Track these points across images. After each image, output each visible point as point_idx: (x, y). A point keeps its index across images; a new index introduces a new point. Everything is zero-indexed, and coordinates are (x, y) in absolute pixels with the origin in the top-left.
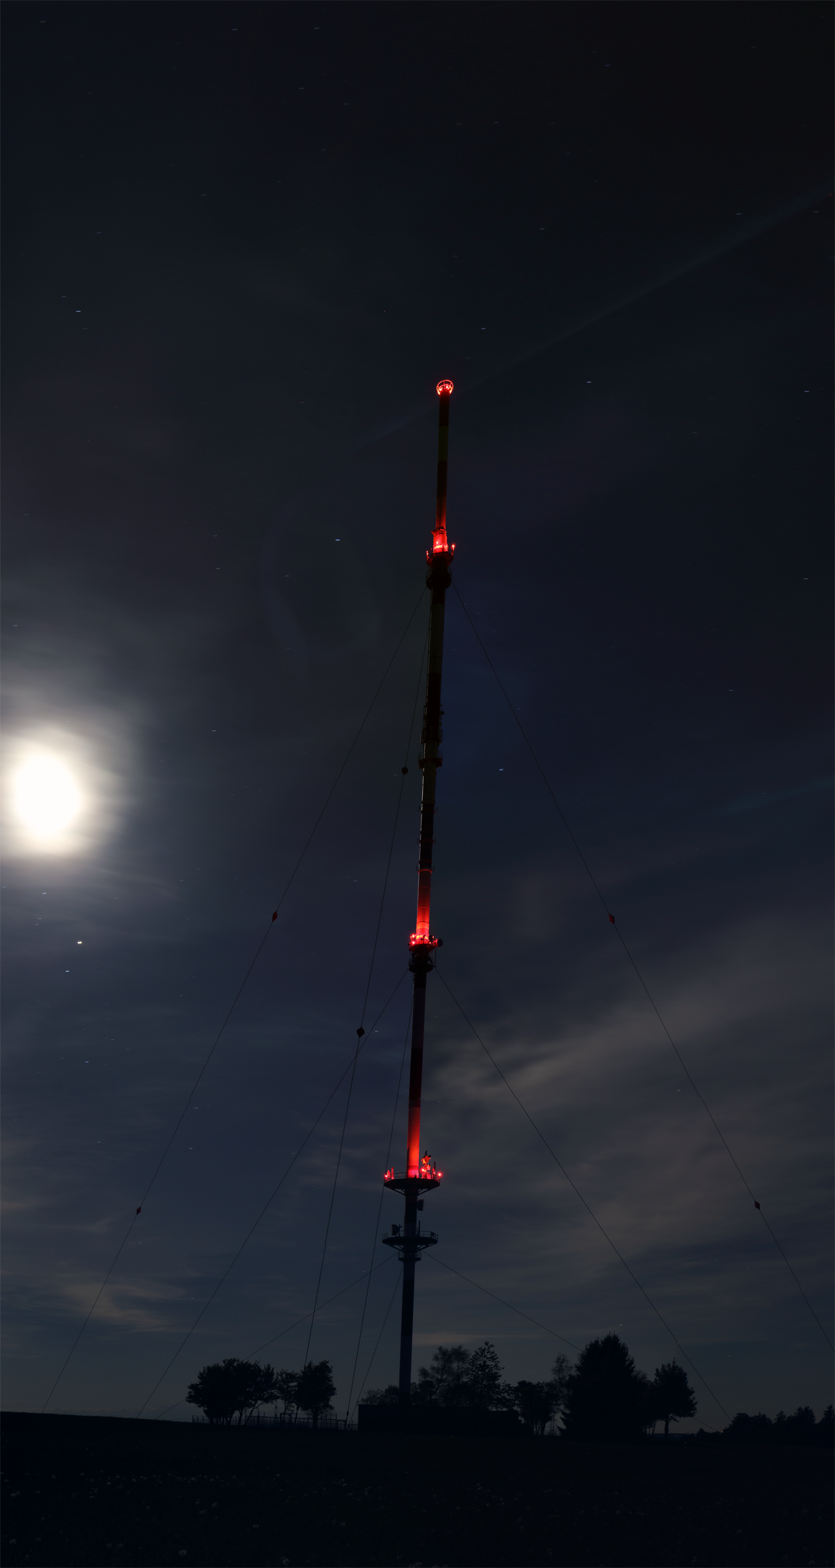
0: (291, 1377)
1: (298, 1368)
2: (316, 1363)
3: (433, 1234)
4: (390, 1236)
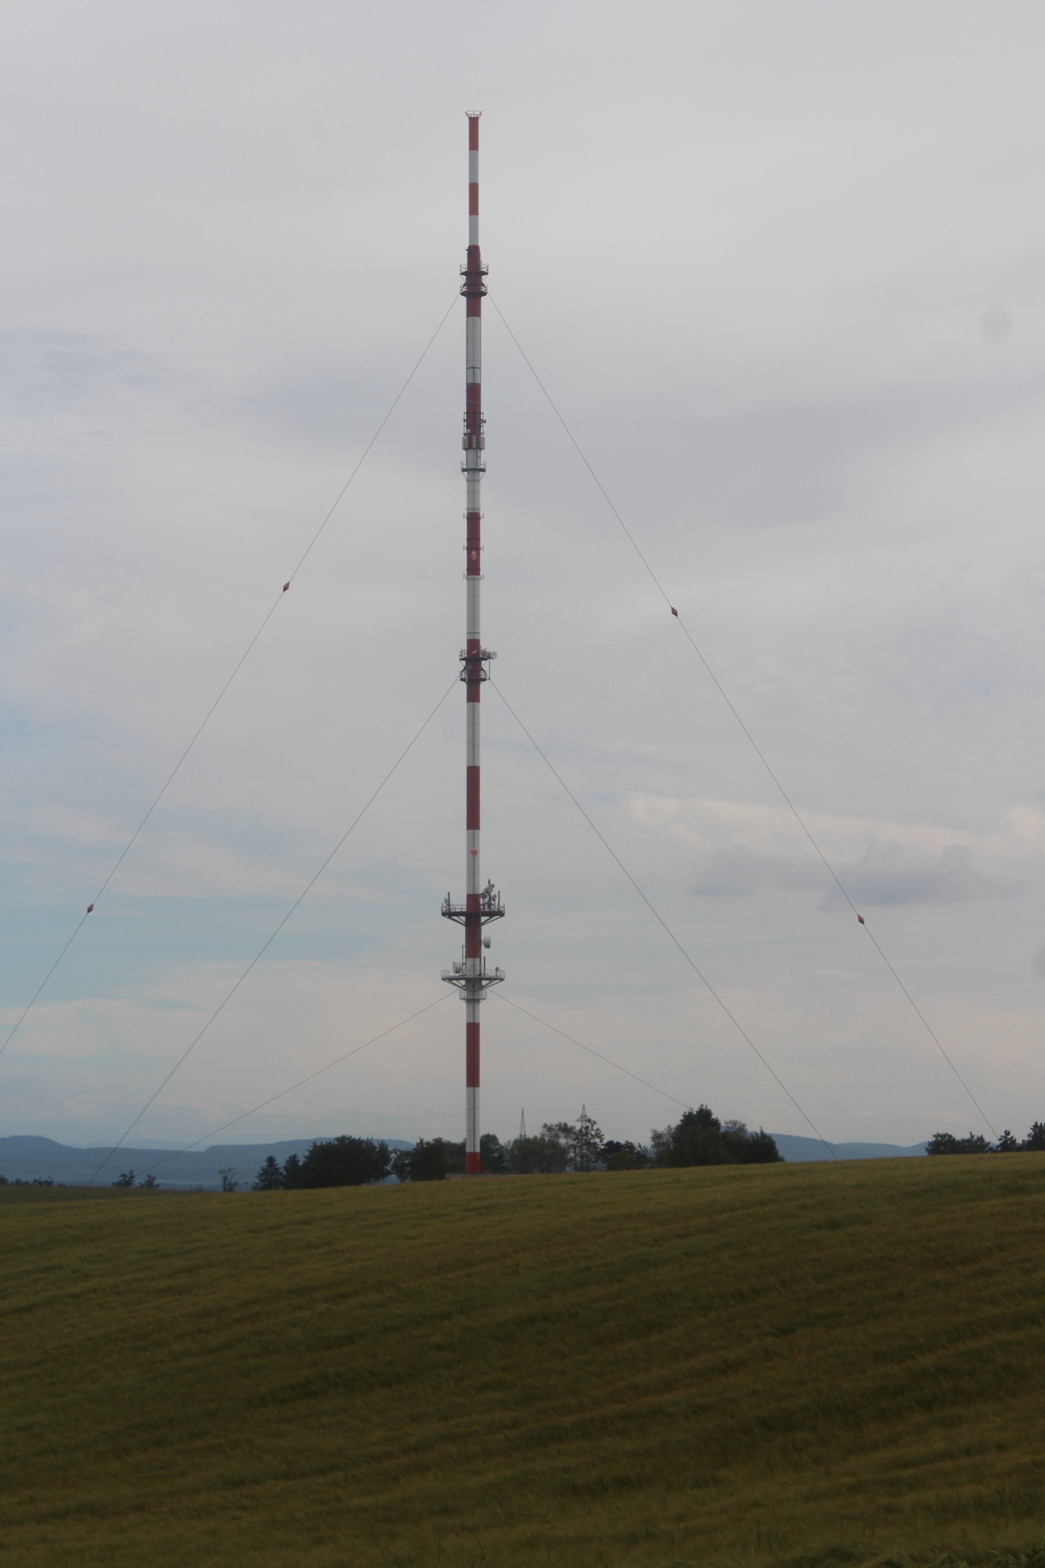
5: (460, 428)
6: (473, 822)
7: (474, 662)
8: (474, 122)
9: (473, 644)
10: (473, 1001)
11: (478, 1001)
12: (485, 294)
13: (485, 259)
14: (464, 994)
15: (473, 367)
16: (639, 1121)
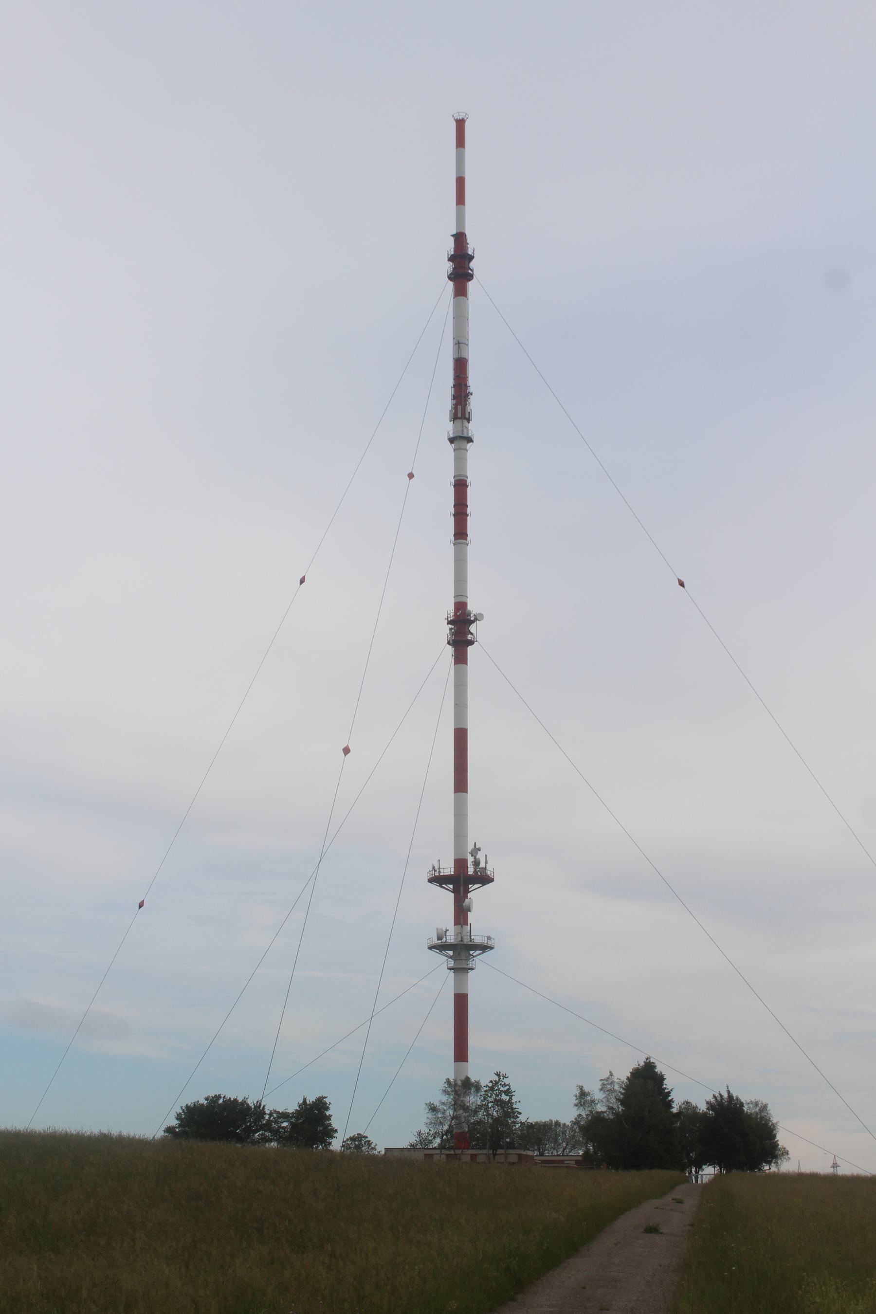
0: (284, 1116)
1: (292, 1107)
2: (311, 1099)
3: (489, 938)
4: (435, 941)
5: (447, 403)
6: (461, 784)
7: (461, 629)
8: (460, 124)
9: (461, 606)
10: (460, 970)
11: (467, 970)
12: (471, 643)
13: (473, 245)
14: (451, 963)
15: (460, 343)
16: (146, 1115)
